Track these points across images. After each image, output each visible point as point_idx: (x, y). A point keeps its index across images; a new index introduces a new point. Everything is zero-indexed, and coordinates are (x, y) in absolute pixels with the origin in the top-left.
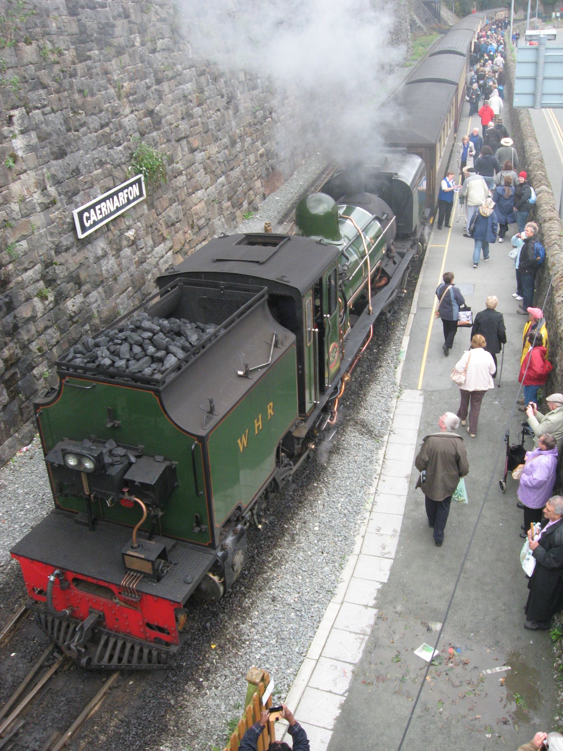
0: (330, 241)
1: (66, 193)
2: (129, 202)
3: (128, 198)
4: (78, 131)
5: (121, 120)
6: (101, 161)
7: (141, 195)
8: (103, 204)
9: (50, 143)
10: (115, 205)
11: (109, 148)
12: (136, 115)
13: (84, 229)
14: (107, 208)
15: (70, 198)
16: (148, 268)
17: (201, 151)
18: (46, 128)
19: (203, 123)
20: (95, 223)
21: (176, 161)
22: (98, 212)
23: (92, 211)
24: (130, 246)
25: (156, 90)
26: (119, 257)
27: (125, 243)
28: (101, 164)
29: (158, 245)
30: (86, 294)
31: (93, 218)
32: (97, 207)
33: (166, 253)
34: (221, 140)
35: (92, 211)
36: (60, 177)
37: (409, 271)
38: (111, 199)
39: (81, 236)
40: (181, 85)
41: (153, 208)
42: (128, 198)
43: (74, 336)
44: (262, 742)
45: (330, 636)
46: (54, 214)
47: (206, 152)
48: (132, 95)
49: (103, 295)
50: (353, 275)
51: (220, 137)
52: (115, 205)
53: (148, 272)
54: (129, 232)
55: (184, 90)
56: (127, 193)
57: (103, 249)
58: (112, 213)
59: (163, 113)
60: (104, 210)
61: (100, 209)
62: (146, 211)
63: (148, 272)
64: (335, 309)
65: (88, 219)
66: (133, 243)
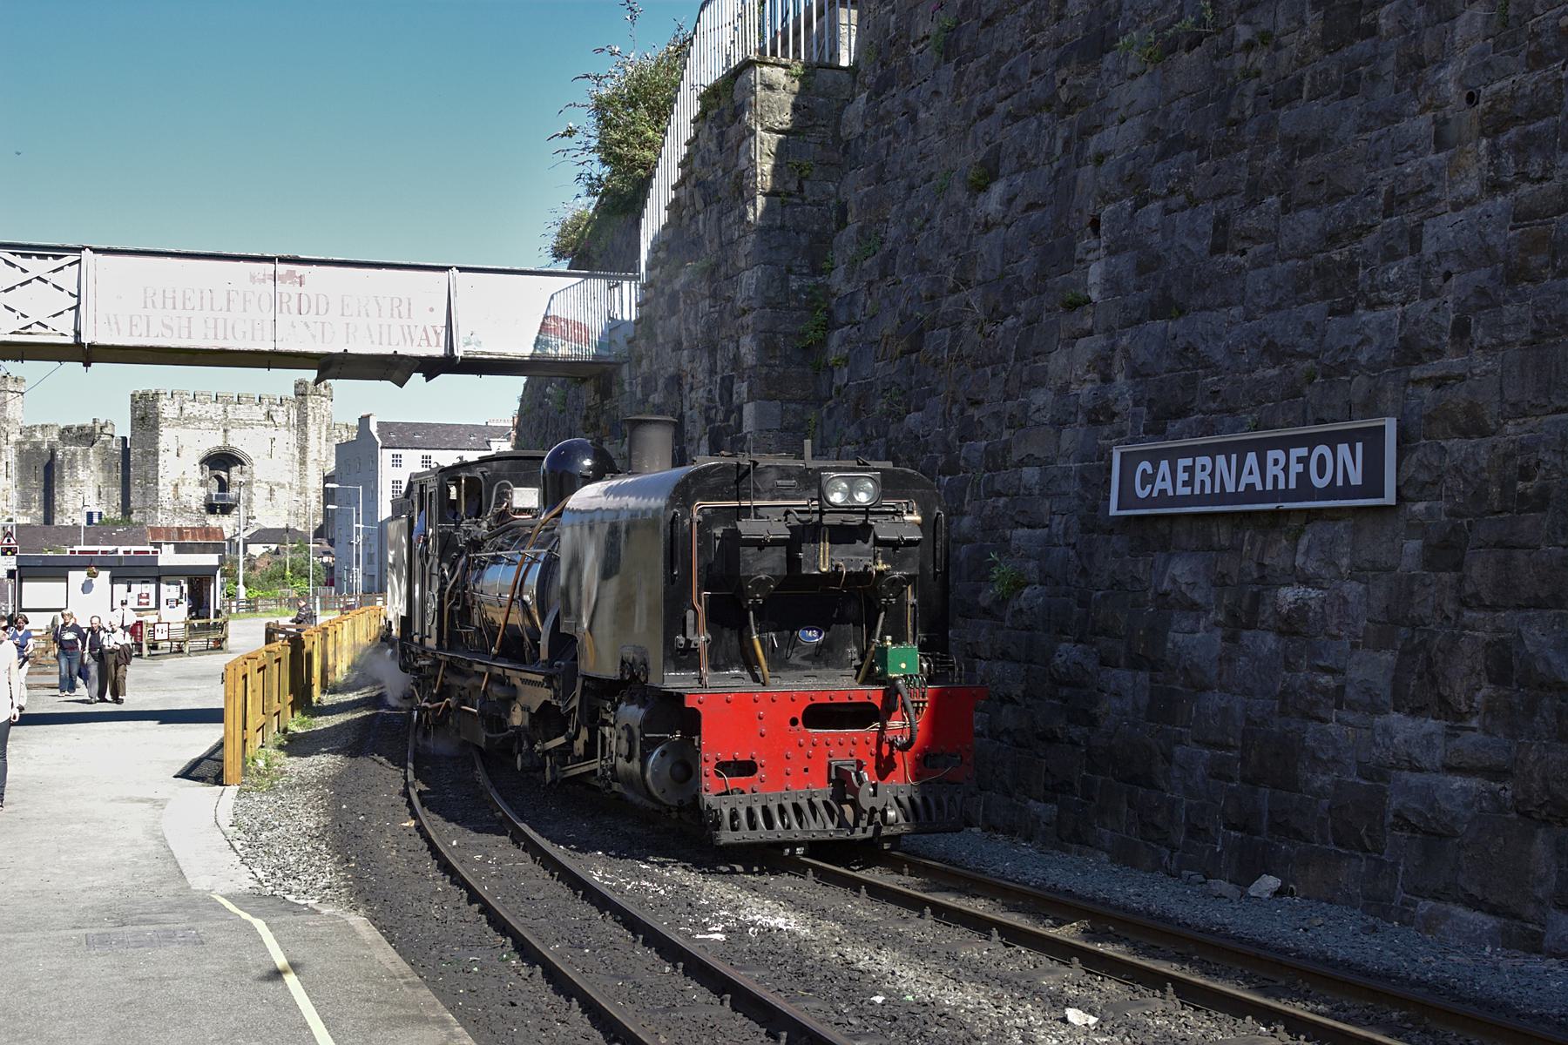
2: (1305, 488)
3: (1303, 477)
27: (1266, 613)
28: (1275, 352)
42: (1303, 477)
52: (1245, 479)
58: (1223, 497)
66: (1292, 625)
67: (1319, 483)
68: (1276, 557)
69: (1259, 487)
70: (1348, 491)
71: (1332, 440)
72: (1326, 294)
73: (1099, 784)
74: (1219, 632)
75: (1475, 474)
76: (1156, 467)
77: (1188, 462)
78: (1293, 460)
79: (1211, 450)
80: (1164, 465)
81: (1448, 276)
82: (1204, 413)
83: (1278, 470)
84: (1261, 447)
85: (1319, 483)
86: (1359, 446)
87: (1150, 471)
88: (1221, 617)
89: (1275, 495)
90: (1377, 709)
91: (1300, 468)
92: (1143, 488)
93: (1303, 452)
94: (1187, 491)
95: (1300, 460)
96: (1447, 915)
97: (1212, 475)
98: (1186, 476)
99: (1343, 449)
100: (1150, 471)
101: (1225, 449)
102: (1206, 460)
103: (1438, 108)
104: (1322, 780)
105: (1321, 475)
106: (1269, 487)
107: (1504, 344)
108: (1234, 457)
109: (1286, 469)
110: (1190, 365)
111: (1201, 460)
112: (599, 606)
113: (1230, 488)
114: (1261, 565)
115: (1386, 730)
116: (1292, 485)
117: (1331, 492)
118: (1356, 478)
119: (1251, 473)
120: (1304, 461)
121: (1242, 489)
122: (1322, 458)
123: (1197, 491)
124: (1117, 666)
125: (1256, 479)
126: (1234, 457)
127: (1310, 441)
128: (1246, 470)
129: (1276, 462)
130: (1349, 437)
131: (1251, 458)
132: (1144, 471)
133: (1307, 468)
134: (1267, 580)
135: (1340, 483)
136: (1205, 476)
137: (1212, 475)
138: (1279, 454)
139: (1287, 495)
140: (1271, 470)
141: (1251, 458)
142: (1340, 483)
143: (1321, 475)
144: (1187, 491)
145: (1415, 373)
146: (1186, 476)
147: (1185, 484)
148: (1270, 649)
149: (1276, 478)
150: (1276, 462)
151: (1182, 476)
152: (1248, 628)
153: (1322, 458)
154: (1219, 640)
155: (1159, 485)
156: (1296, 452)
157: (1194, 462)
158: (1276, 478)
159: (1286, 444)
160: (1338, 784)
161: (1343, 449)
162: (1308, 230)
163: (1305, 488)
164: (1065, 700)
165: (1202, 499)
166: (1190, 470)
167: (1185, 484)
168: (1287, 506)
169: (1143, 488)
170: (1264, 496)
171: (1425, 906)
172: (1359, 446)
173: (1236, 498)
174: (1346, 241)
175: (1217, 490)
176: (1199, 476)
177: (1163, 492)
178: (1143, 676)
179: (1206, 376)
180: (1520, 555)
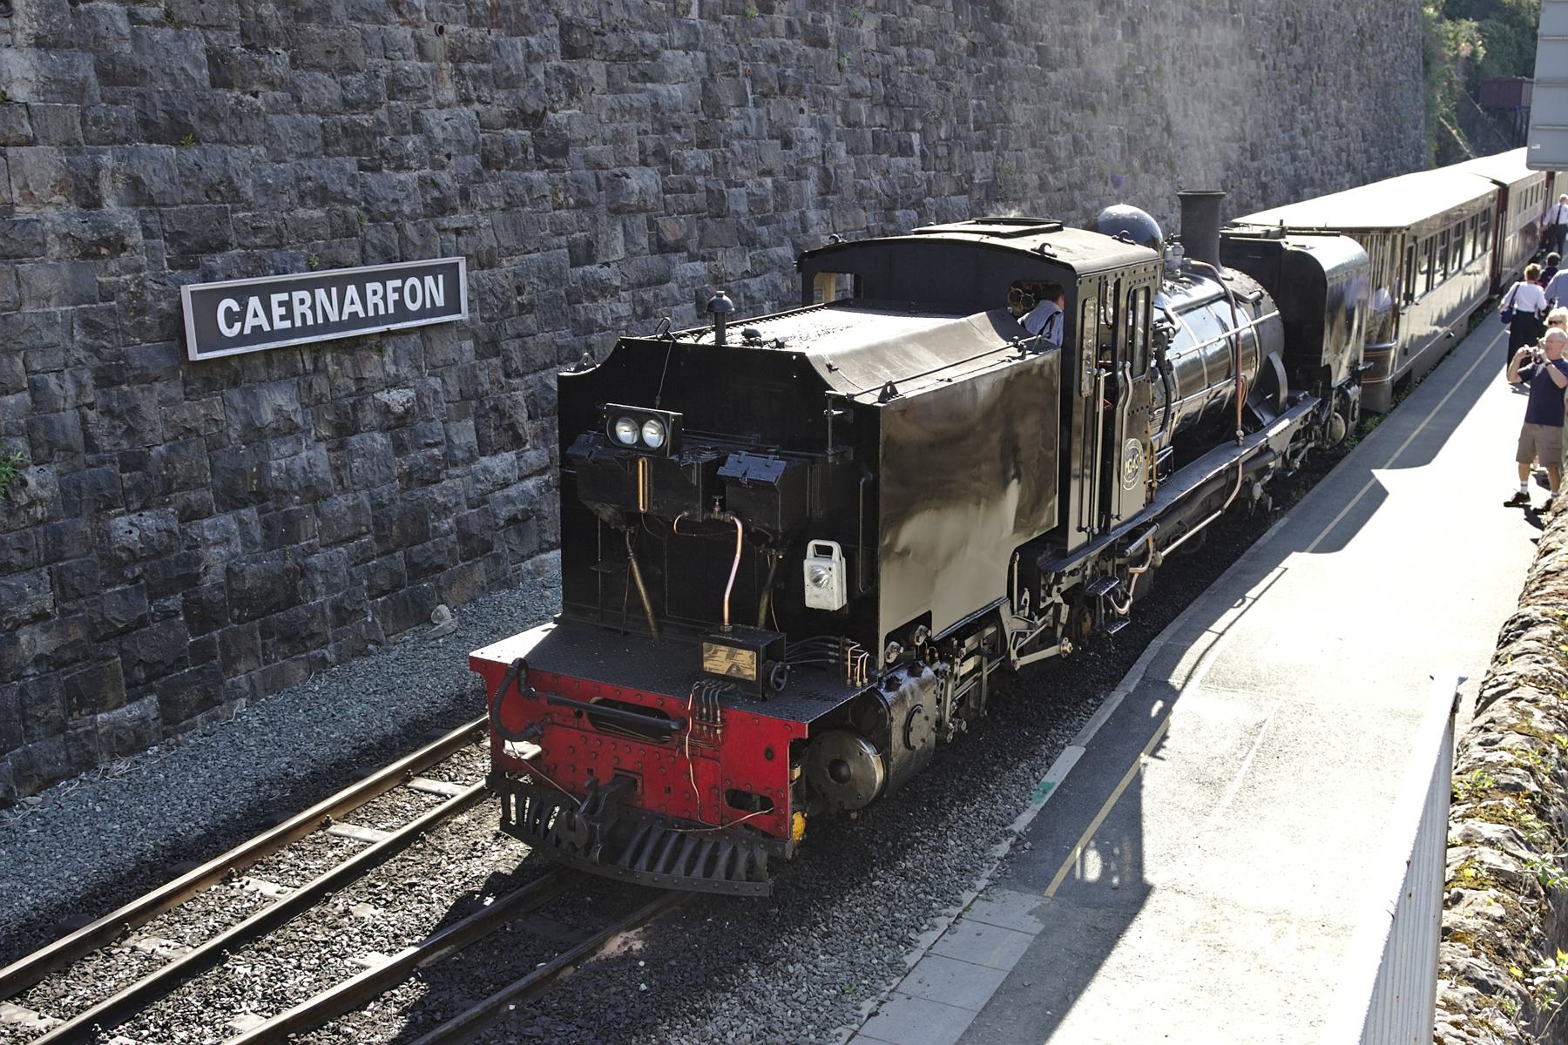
1: (174, 238)
2: (402, 312)
3: (400, 304)
5: (423, 111)
6: (324, 188)
7: (453, 305)
9: (140, 95)
11: (362, 167)
12: (478, 114)
15: (185, 253)
16: (441, 500)
17: (692, 258)
18: (136, 57)
19: (708, 190)
21: (602, 259)
24: (389, 429)
25: (560, 70)
26: (342, 446)
27: (369, 416)
28: (322, 195)
29: (495, 453)
30: (189, 515)
33: (522, 478)
34: (764, 246)
36: (155, 190)
39: (195, 355)
40: (652, 80)
41: (497, 355)
42: (400, 304)
43: (114, 614)
46: (110, 273)
47: (713, 263)
48: (475, 60)
49: (257, 533)
50: (648, 607)
51: (766, 238)
52: (347, 309)
53: (444, 510)
54: (394, 392)
55: (655, 95)
56: (400, 290)
57: (278, 411)
58: (328, 326)
59: (578, 132)
62: (469, 356)
63: (444, 510)
64: (1347, 344)
66: (397, 424)
67: (413, 307)
68: (373, 369)
69: (362, 315)
70: (436, 311)
71: (420, 273)
72: (355, 151)
73: (218, 640)
74: (322, 447)
75: (503, 294)
76: (244, 306)
77: (284, 297)
78: (389, 290)
79: (310, 285)
80: (254, 302)
81: (449, 156)
82: (245, 248)
83: (378, 299)
84: (360, 281)
85: (413, 307)
86: (441, 277)
87: (236, 308)
88: (325, 433)
89: (377, 320)
90: (472, 459)
91: (396, 296)
92: (230, 326)
93: (398, 283)
94: (287, 324)
95: (395, 290)
96: (543, 561)
97: (313, 308)
98: (283, 311)
99: (429, 280)
100: (236, 308)
101: (325, 283)
102: (305, 294)
103: (417, 27)
104: (446, 524)
105: (414, 300)
106: (371, 313)
107: (492, 208)
108: (334, 290)
109: (384, 298)
110: (218, 199)
111: (296, 295)
112: (1450, 365)
113: (333, 317)
114: (359, 380)
115: (485, 470)
116: (391, 310)
117: (422, 313)
118: (440, 302)
119: (352, 303)
120: (400, 290)
121: (345, 317)
122: (413, 288)
123: (298, 323)
124: (210, 515)
125: (358, 307)
126: (334, 290)
127: (404, 275)
128: (348, 301)
129: (375, 292)
130: (433, 271)
131: (351, 290)
132: (228, 310)
133: (401, 296)
134: (363, 388)
135: (428, 305)
136: (306, 309)
137: (313, 308)
138: (378, 286)
139: (387, 319)
140: (371, 299)
141: (351, 290)
142: (428, 305)
143: (414, 300)
144: (287, 324)
145: (445, 222)
146: (283, 311)
147: (282, 318)
148: (382, 445)
149: (376, 306)
150: (375, 292)
151: (278, 311)
152: (355, 433)
153: (413, 288)
154: (325, 453)
155: (251, 321)
156: (391, 284)
157: (290, 296)
158: (376, 306)
159: (382, 277)
160: (458, 522)
161: (429, 280)
162: (331, 93)
163: (402, 312)
164: (136, 580)
165: (305, 330)
166: (288, 305)
167: (282, 318)
168: (393, 327)
169: (230, 326)
170: (368, 322)
171: (528, 565)
172: (441, 277)
173: (340, 326)
174: (360, 110)
175: (320, 321)
176: (298, 309)
177: (257, 329)
178: (250, 514)
179: (234, 211)
180: (529, 340)
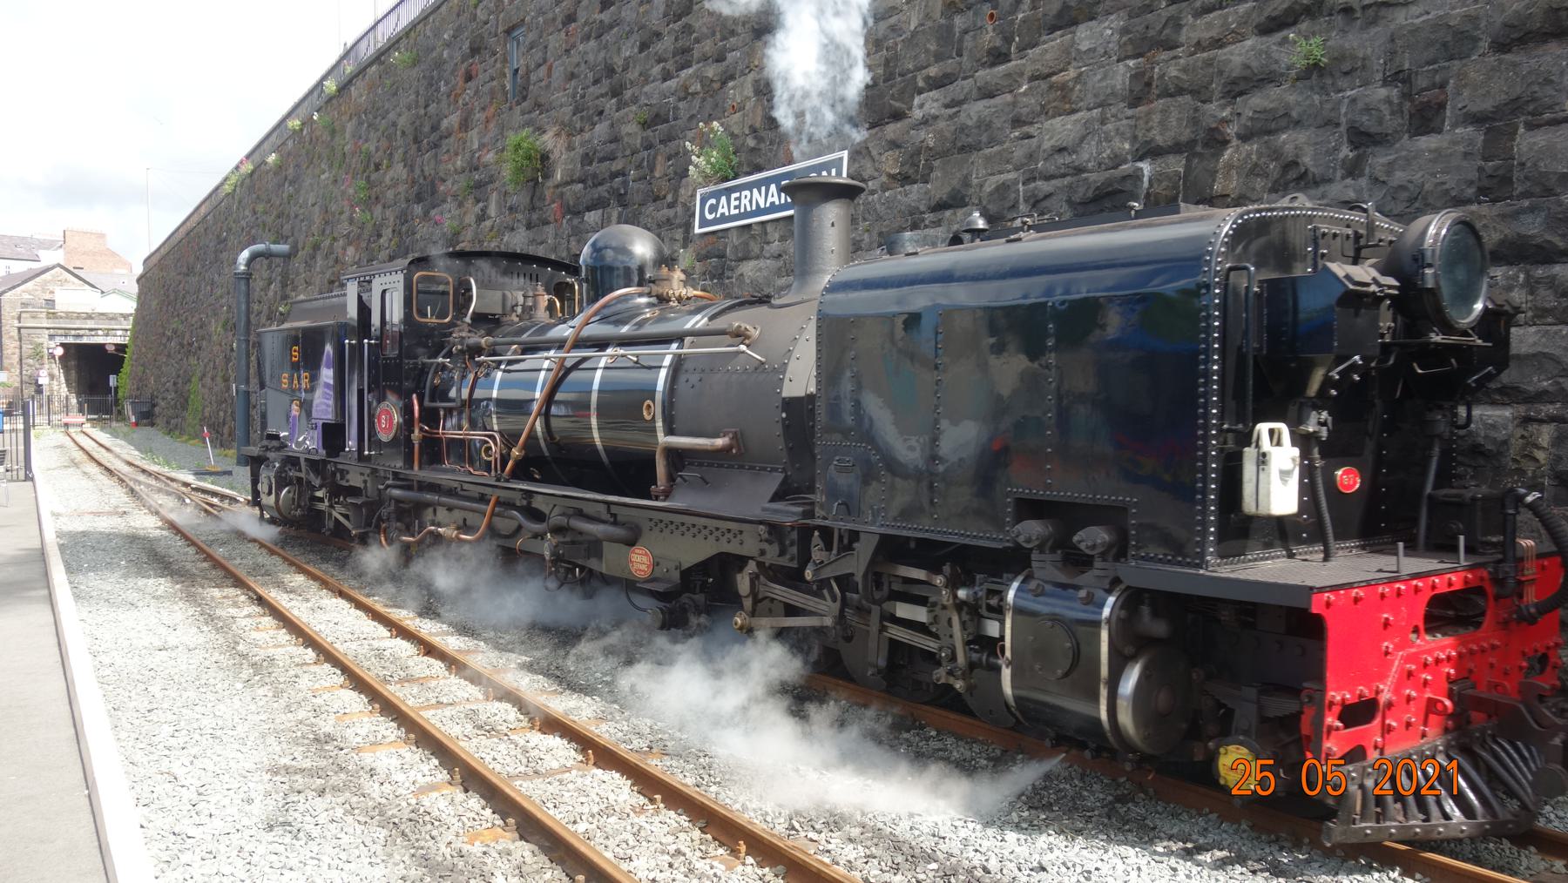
0: (1146, 179)
4: (898, 116)
8: (747, 193)
10: (770, 200)
13: (704, 223)
14: (751, 201)
20: (724, 219)
22: (734, 203)
23: (723, 199)
31: (723, 210)
32: (734, 196)
35: (723, 199)
37: (1307, 557)
38: (763, 188)
44: (188, 224)
45: (56, 649)
52: (770, 200)
60: (745, 202)
61: (739, 199)
65: (713, 209)
